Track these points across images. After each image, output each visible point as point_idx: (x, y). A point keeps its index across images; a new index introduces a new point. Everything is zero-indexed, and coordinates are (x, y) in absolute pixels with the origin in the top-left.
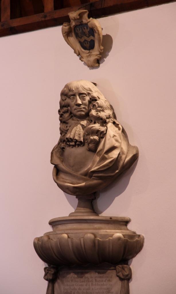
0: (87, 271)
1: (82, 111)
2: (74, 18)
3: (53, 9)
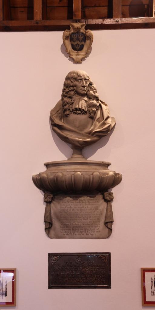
0: (80, 196)
1: (85, 91)
2: (77, 27)
3: (42, 19)
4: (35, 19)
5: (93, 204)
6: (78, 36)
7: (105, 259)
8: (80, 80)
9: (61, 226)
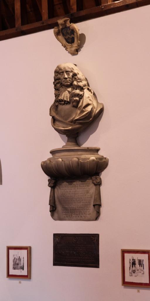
3: (48, 18)
4: (43, 19)
5: (83, 187)
6: (66, 31)
7: (95, 240)
8: (61, 73)
9: (62, 209)
